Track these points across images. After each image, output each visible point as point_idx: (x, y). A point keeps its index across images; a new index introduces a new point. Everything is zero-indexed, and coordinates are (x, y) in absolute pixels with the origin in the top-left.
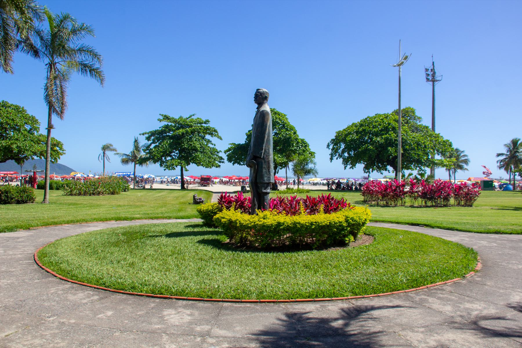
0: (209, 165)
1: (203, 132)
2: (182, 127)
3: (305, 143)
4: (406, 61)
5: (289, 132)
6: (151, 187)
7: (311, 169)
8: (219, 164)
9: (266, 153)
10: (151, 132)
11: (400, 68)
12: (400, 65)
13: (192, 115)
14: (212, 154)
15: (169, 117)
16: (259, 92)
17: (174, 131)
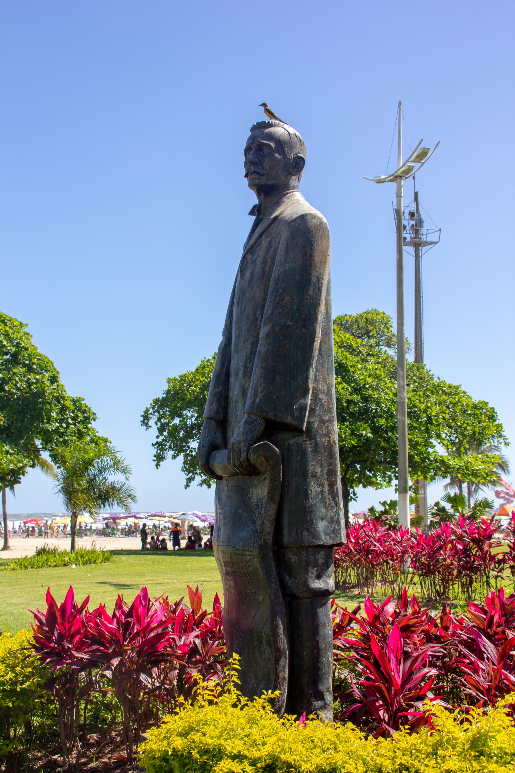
3: (84, 412)
4: (420, 164)
5: (37, 377)
7: (113, 488)
11: (399, 187)
12: (401, 177)
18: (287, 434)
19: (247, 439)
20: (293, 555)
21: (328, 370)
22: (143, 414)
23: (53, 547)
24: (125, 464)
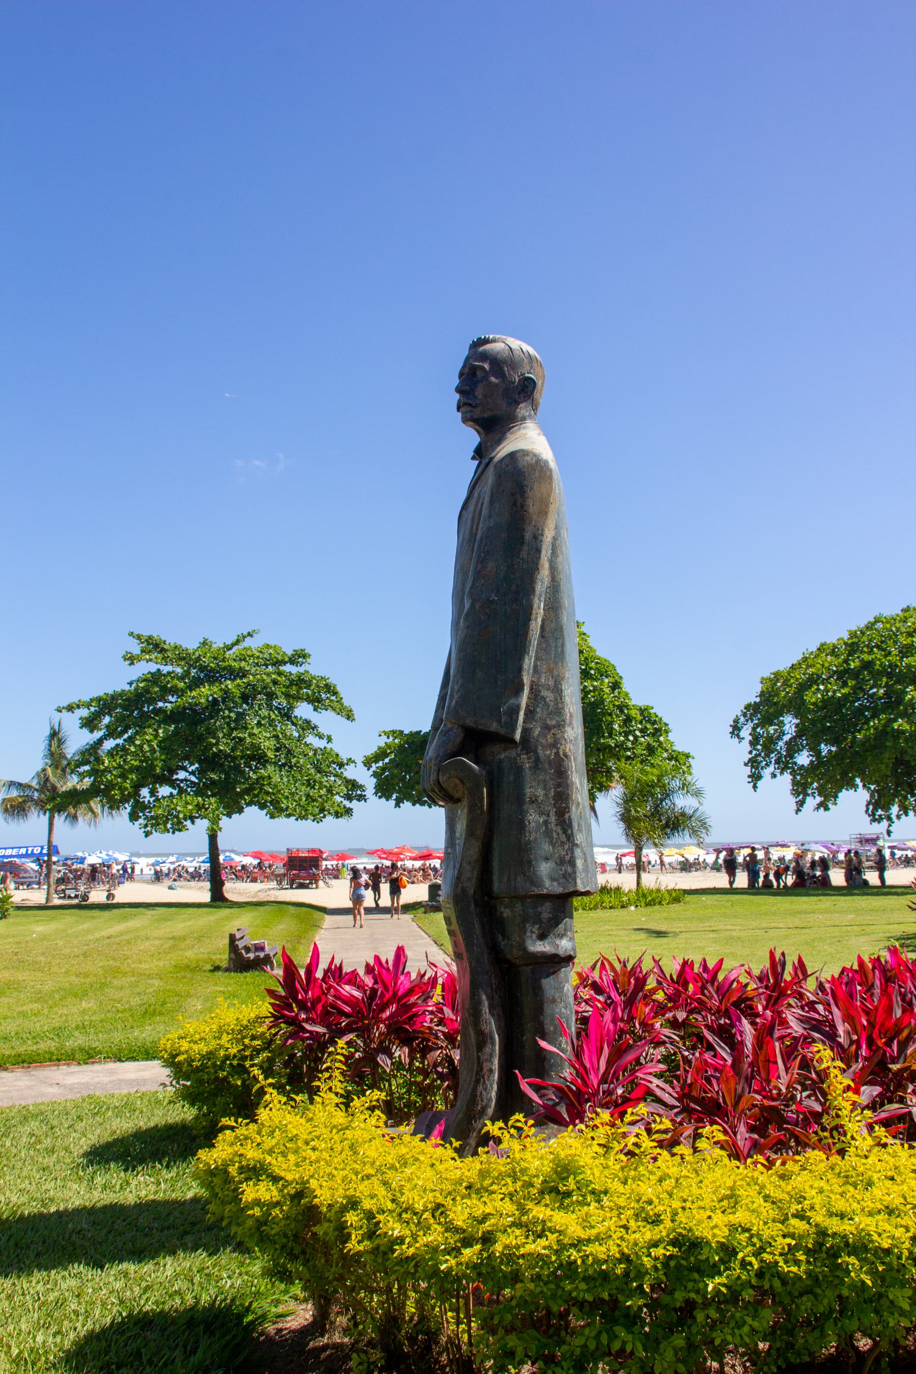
0: (310, 808)
1: (287, 696)
2: (211, 675)
3: (655, 722)
5: (595, 683)
6: (108, 897)
7: (683, 814)
8: (347, 803)
9: (540, 712)
10: (99, 699)
13: (245, 634)
14: (319, 772)
15: (162, 645)
16: (485, 357)
19: (438, 756)
22: (732, 723)
23: (616, 886)
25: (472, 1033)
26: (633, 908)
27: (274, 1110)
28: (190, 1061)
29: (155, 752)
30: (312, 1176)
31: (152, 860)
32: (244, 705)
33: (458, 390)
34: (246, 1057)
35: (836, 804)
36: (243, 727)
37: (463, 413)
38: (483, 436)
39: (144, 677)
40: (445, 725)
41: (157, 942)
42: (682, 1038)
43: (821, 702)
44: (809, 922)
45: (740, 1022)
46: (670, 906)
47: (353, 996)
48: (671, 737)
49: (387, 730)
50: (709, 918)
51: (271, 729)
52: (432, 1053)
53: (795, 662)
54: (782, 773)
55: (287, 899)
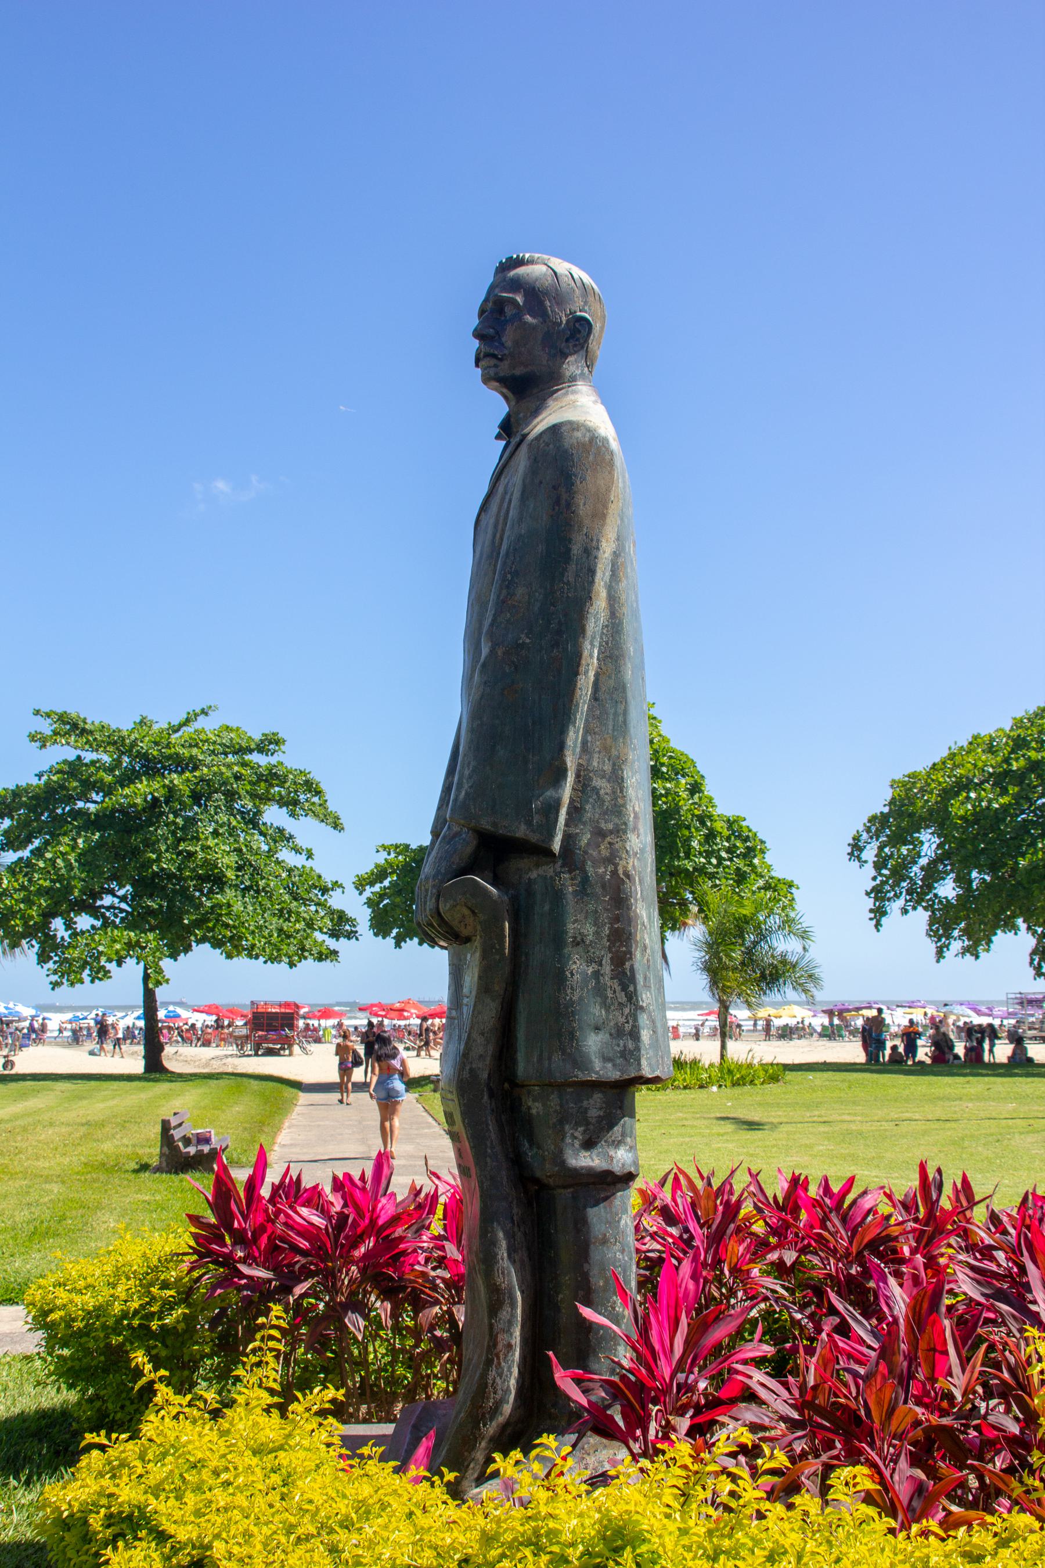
0: (285, 947)
1: (253, 796)
2: (151, 767)
3: (747, 839)
5: (668, 785)
7: (784, 962)
8: (332, 943)
9: (590, 811)
13: (198, 711)
14: (296, 899)
16: (516, 285)
17: (108, 791)
18: (526, 860)
19: (438, 872)
20: (534, 1101)
21: (614, 730)
22: (851, 842)
23: (692, 1057)
24: (804, 925)
25: (482, 1289)
26: (715, 1089)
27: (167, 1420)
28: (69, 1320)
29: (72, 869)
30: (217, 1536)
31: (69, 1016)
32: (195, 808)
33: (478, 334)
34: (153, 1314)
35: (988, 951)
36: (193, 838)
37: (484, 369)
38: (513, 403)
39: (58, 767)
40: (449, 828)
41: (64, 1130)
42: (791, 1291)
43: (972, 815)
44: (955, 1112)
45: (886, 1282)
46: (766, 1086)
47: (313, 1224)
48: (769, 858)
49: (387, 843)
50: (818, 1105)
51: (232, 840)
52: (427, 1311)
53: (937, 760)
54: (914, 908)
55: (250, 1070)
